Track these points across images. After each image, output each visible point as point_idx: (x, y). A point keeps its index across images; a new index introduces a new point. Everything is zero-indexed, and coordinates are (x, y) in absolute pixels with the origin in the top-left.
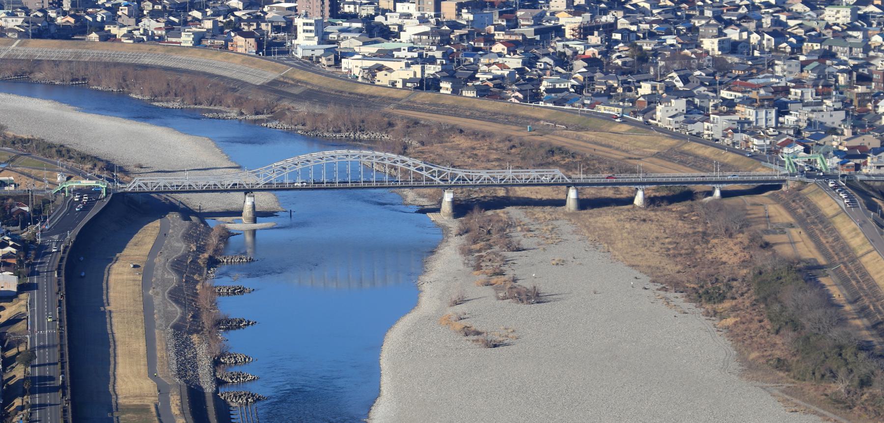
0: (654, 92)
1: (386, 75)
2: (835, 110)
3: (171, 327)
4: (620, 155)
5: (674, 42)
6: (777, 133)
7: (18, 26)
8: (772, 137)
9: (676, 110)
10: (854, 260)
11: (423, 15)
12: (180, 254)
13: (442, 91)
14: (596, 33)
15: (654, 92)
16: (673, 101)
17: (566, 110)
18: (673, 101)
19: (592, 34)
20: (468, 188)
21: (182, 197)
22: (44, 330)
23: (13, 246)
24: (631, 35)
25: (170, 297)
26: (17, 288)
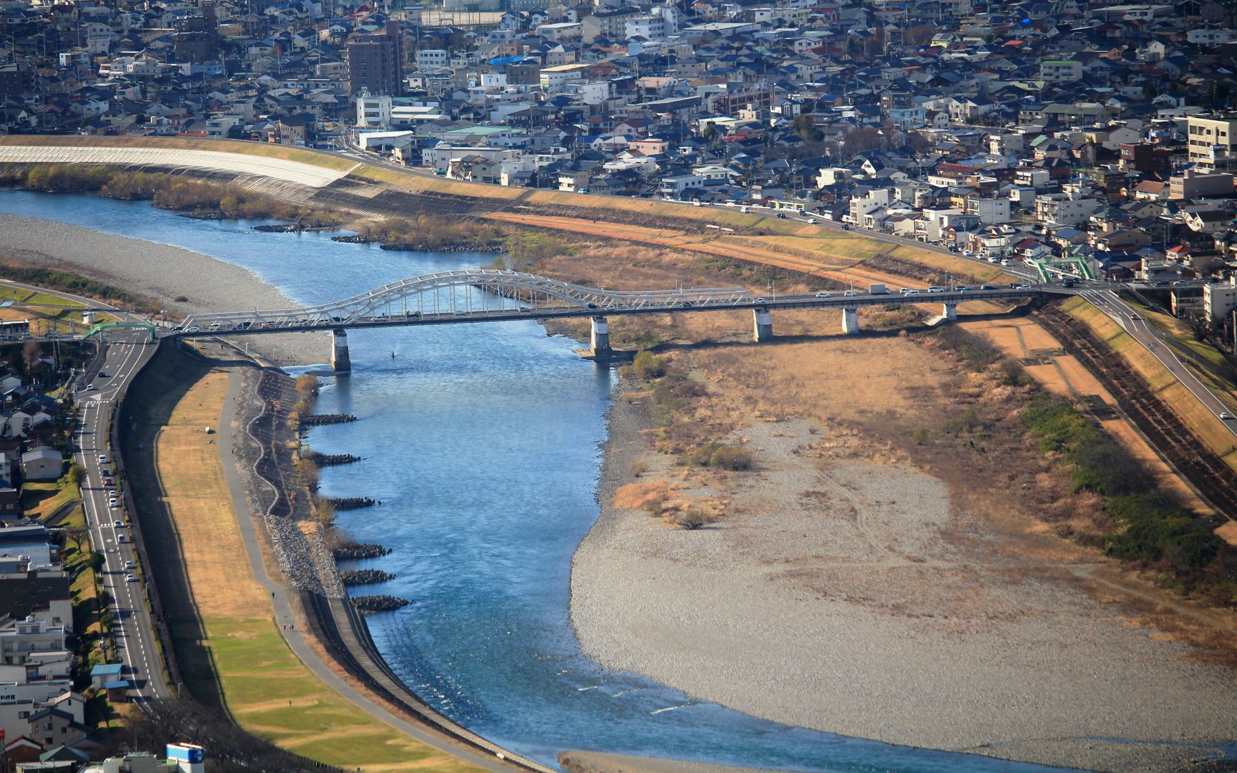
0: (840, 181)
1: (484, 169)
2: (1084, 198)
3: (271, 513)
4: (776, 249)
5: (851, 114)
6: (1013, 231)
7: (361, 217)
8: (1008, 236)
9: (876, 204)
10: (1149, 396)
11: (837, 218)
12: (261, 415)
13: (561, 188)
14: (749, 106)
15: (840, 181)
16: (871, 192)
17: (729, 208)
18: (871, 192)
19: (744, 108)
20: (648, 319)
21: (263, 341)
22: (108, 522)
23: (46, 412)
24: (794, 107)
25: (261, 473)
26: (1218, 536)
